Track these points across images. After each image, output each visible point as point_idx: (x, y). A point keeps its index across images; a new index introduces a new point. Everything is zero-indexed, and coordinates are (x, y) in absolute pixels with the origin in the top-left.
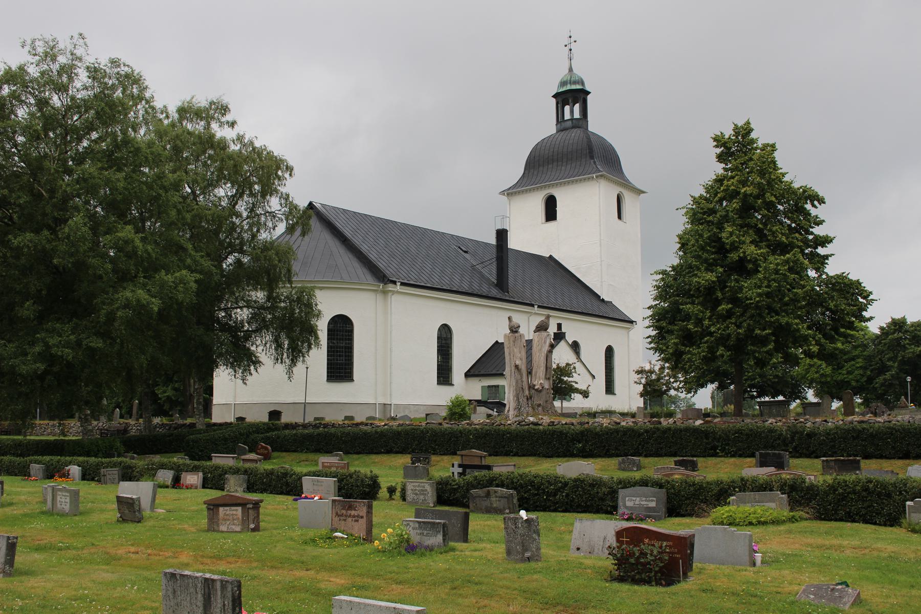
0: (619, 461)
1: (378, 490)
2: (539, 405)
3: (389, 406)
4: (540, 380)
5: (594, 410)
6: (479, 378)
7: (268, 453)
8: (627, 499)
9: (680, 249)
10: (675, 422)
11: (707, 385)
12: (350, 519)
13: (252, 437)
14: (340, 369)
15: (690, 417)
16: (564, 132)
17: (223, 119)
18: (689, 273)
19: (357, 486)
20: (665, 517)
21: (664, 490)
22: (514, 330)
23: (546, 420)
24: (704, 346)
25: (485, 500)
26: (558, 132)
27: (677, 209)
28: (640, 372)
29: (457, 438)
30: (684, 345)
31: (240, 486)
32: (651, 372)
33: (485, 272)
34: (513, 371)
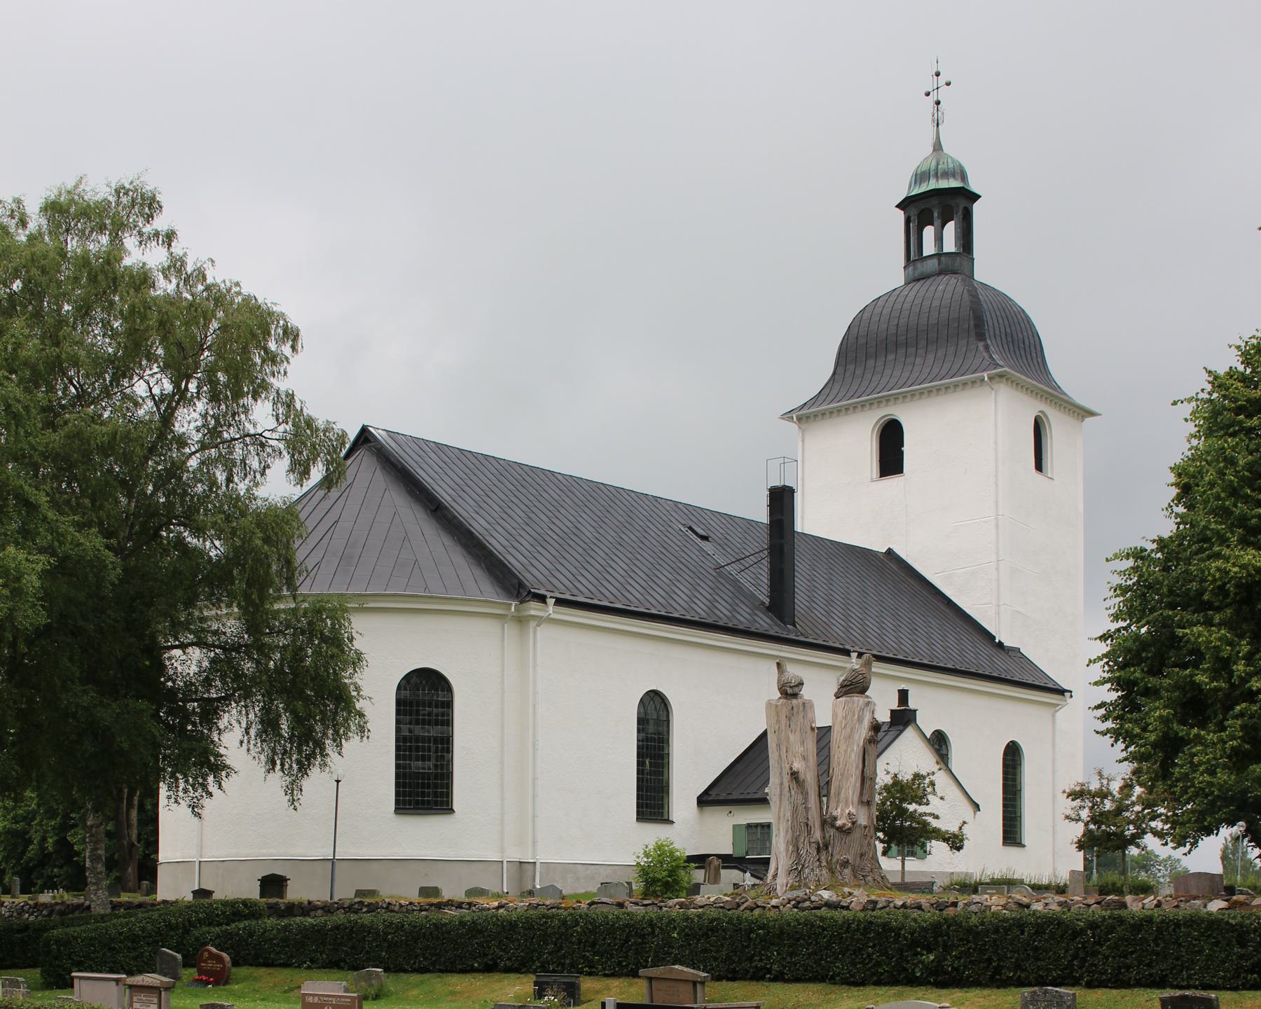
0: (1024, 998)
2: (845, 864)
4: (847, 805)
5: (977, 877)
6: (726, 809)
9: (1178, 499)
10: (1159, 905)
11: (1218, 830)
13: (196, 933)
14: (423, 786)
15: (1194, 892)
16: (921, 282)
17: (147, 229)
22: (789, 691)
23: (859, 897)
26: (907, 283)
27: (1175, 403)
29: (643, 936)
30: (1183, 722)
32: (1104, 794)
33: (745, 580)
34: (786, 784)
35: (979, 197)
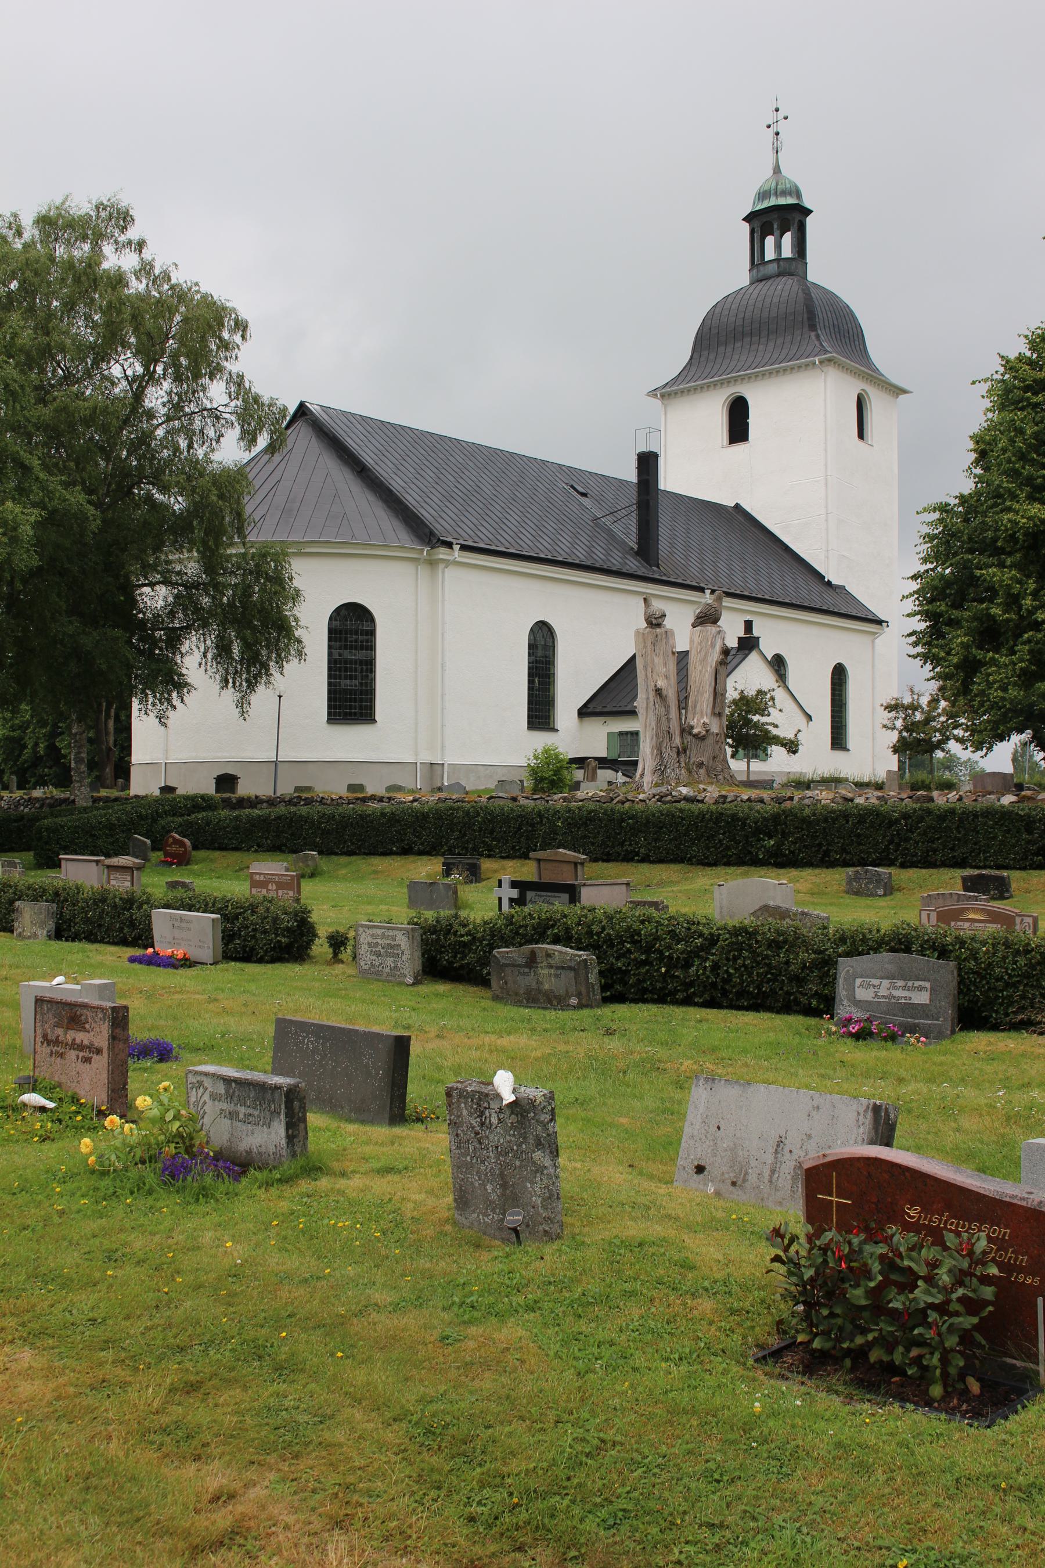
1: (312, 941)
2: (701, 765)
3: (439, 768)
4: (702, 717)
5: (809, 776)
6: (602, 719)
7: (185, 852)
8: (858, 981)
9: (977, 462)
10: (960, 799)
11: (1009, 736)
12: (72, 1054)
14: (351, 700)
15: (989, 788)
18: (996, 505)
19: (265, 932)
20: (953, 1032)
21: (952, 964)
22: (654, 621)
23: (712, 792)
24: (1023, 650)
25: (524, 974)
26: (752, 283)
27: (973, 383)
28: (893, 707)
29: (533, 825)
30: (980, 647)
31: (42, 925)
32: (915, 707)
33: (617, 529)
34: (651, 699)
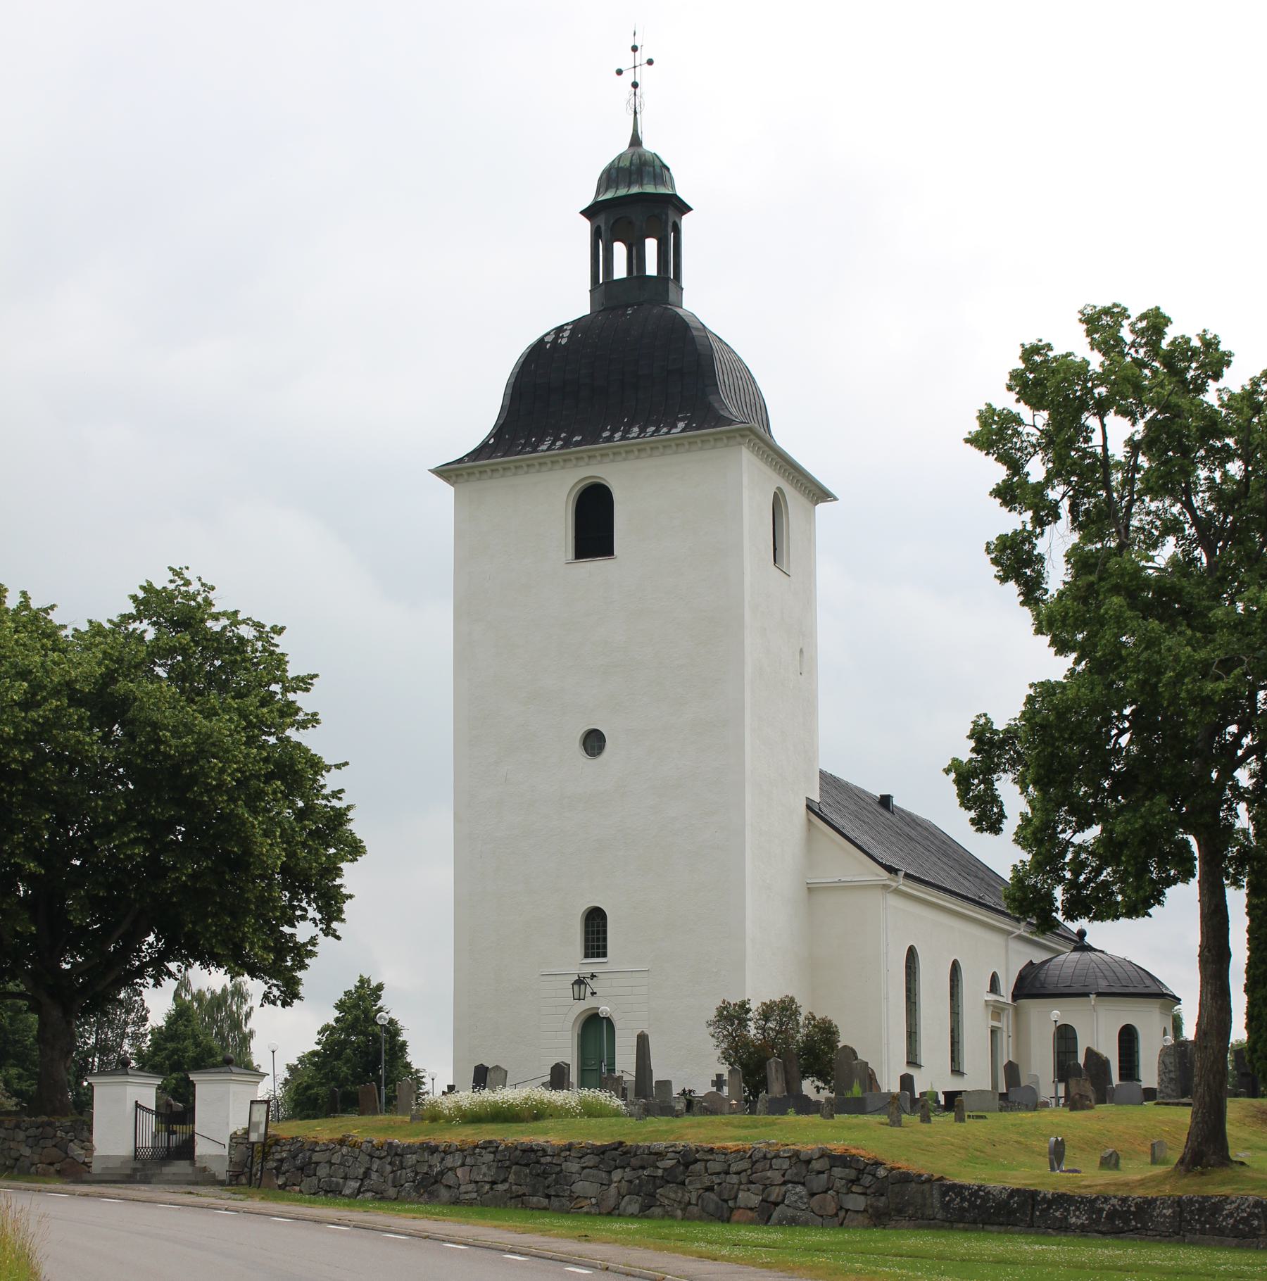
35: (690, 209)
